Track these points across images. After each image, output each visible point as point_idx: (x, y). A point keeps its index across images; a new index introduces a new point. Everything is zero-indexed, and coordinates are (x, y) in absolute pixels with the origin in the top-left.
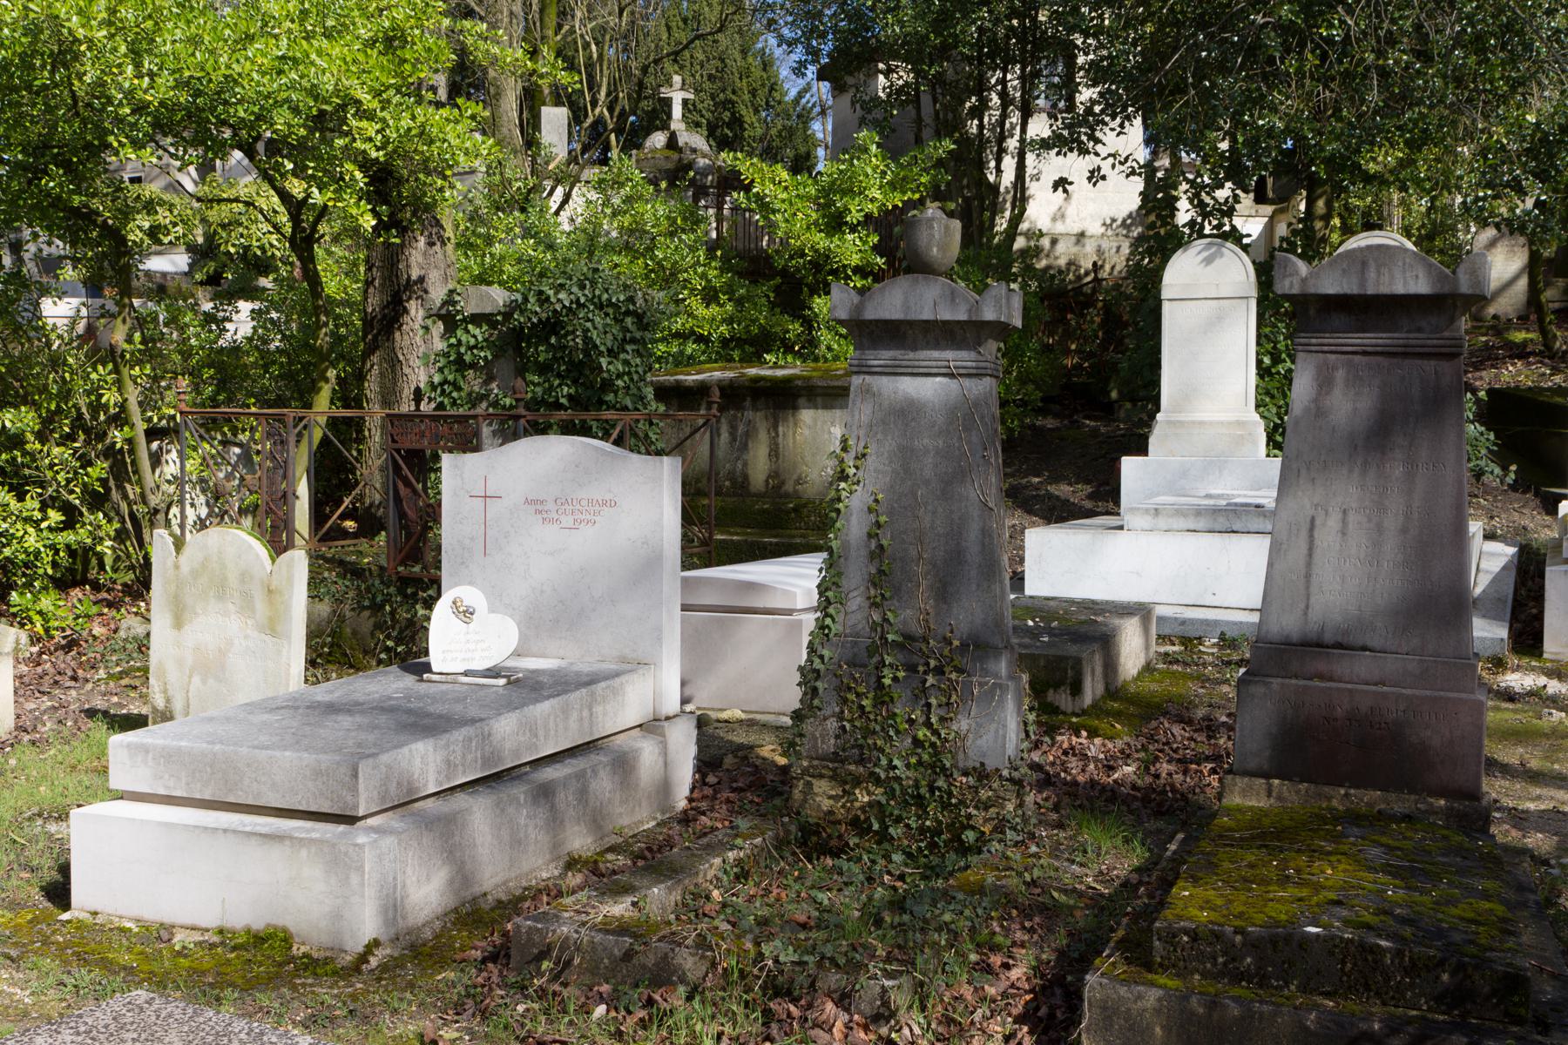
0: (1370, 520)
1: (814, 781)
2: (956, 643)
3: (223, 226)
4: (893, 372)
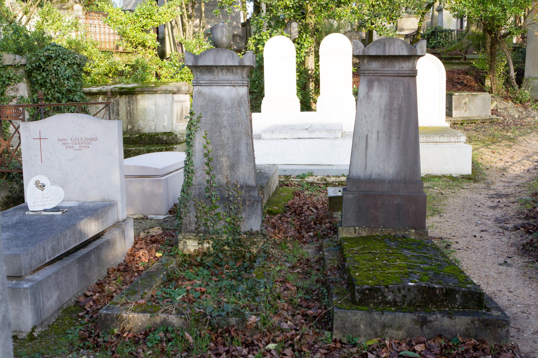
1: (187, 241)
2: (239, 186)
3: (132, 44)
4: (210, 84)
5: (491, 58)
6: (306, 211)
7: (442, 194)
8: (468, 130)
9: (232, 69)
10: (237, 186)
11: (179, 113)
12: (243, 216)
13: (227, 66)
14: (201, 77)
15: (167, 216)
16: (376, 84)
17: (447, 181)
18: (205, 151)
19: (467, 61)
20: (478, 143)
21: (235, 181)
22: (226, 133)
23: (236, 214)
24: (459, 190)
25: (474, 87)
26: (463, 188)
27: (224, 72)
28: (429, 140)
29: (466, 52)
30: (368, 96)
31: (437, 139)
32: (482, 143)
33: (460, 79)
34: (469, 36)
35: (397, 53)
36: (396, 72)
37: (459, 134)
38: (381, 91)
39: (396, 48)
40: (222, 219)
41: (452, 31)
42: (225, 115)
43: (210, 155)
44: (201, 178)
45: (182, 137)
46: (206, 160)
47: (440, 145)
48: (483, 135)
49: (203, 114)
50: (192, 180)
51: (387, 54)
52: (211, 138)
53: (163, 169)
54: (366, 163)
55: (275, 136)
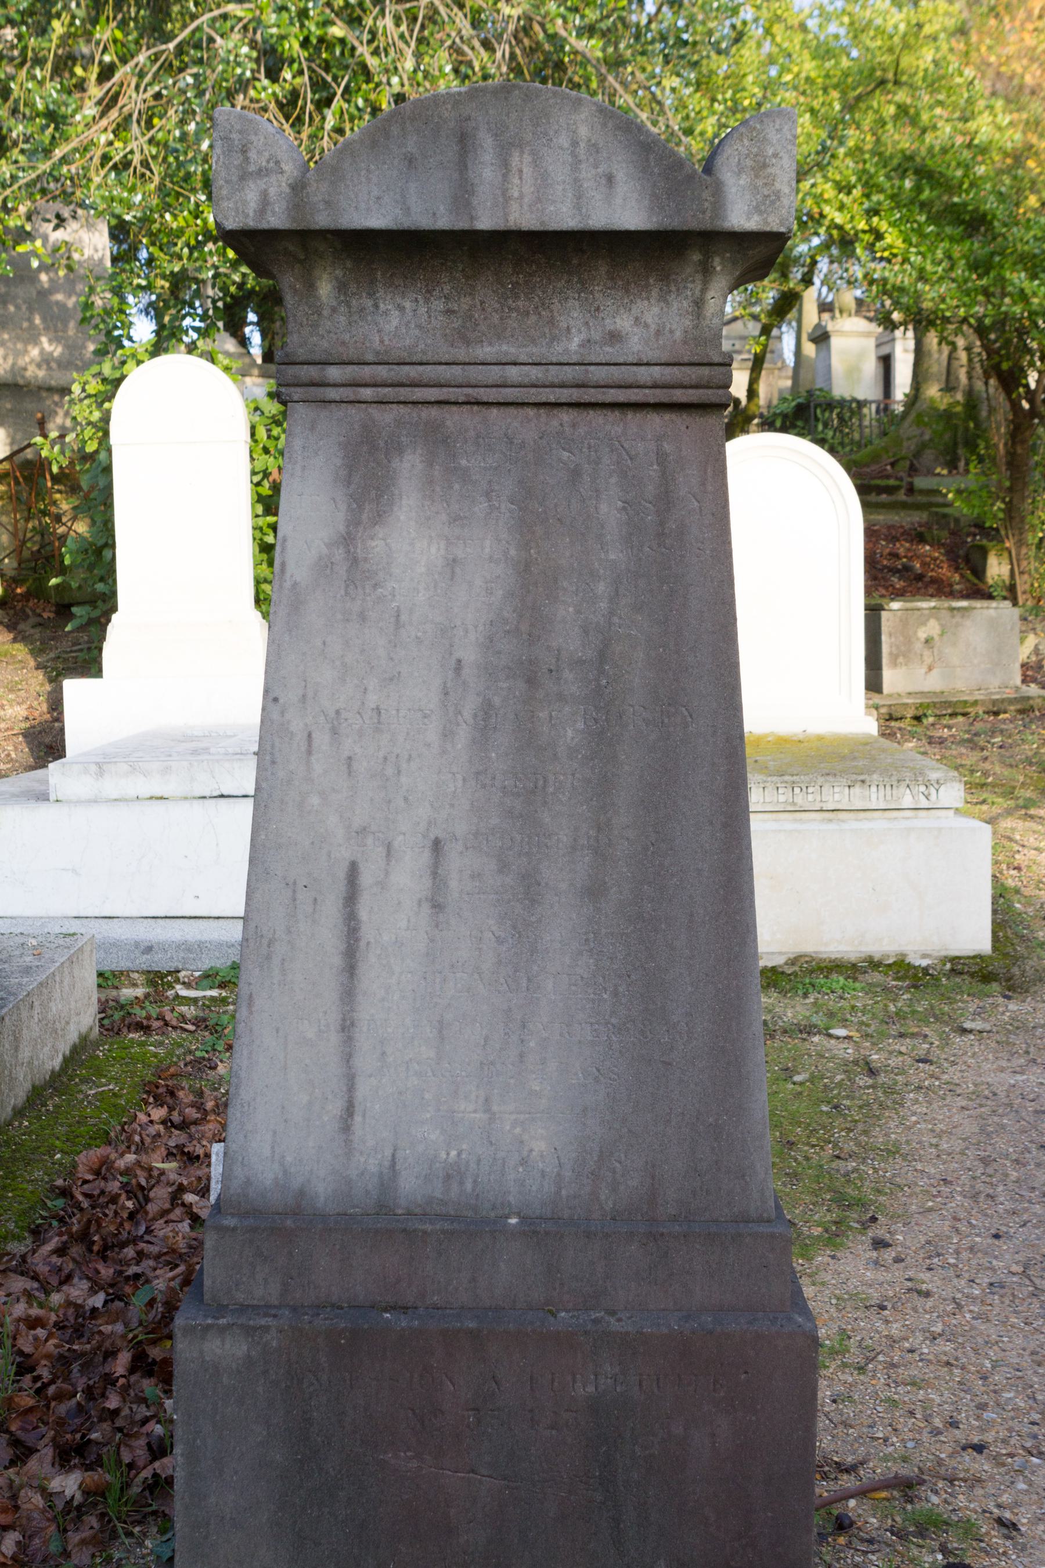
0: (503, 867)
5: (1011, 478)
6: (164, 1213)
7: (872, 1072)
8: (942, 741)
16: (409, 466)
17: (886, 989)
19: (921, 499)
20: (991, 797)
24: (946, 1042)
25: (951, 585)
26: (964, 1031)
28: (800, 799)
29: (913, 470)
30: (352, 564)
31: (837, 795)
32: (1004, 795)
33: (895, 556)
34: (919, 415)
35: (563, 217)
36: (569, 374)
37: (934, 776)
38: (456, 519)
39: (559, 171)
41: (861, 404)
47: (852, 823)
48: (1002, 762)
51: (485, 223)
54: (351, 1088)
55: (110, 787)
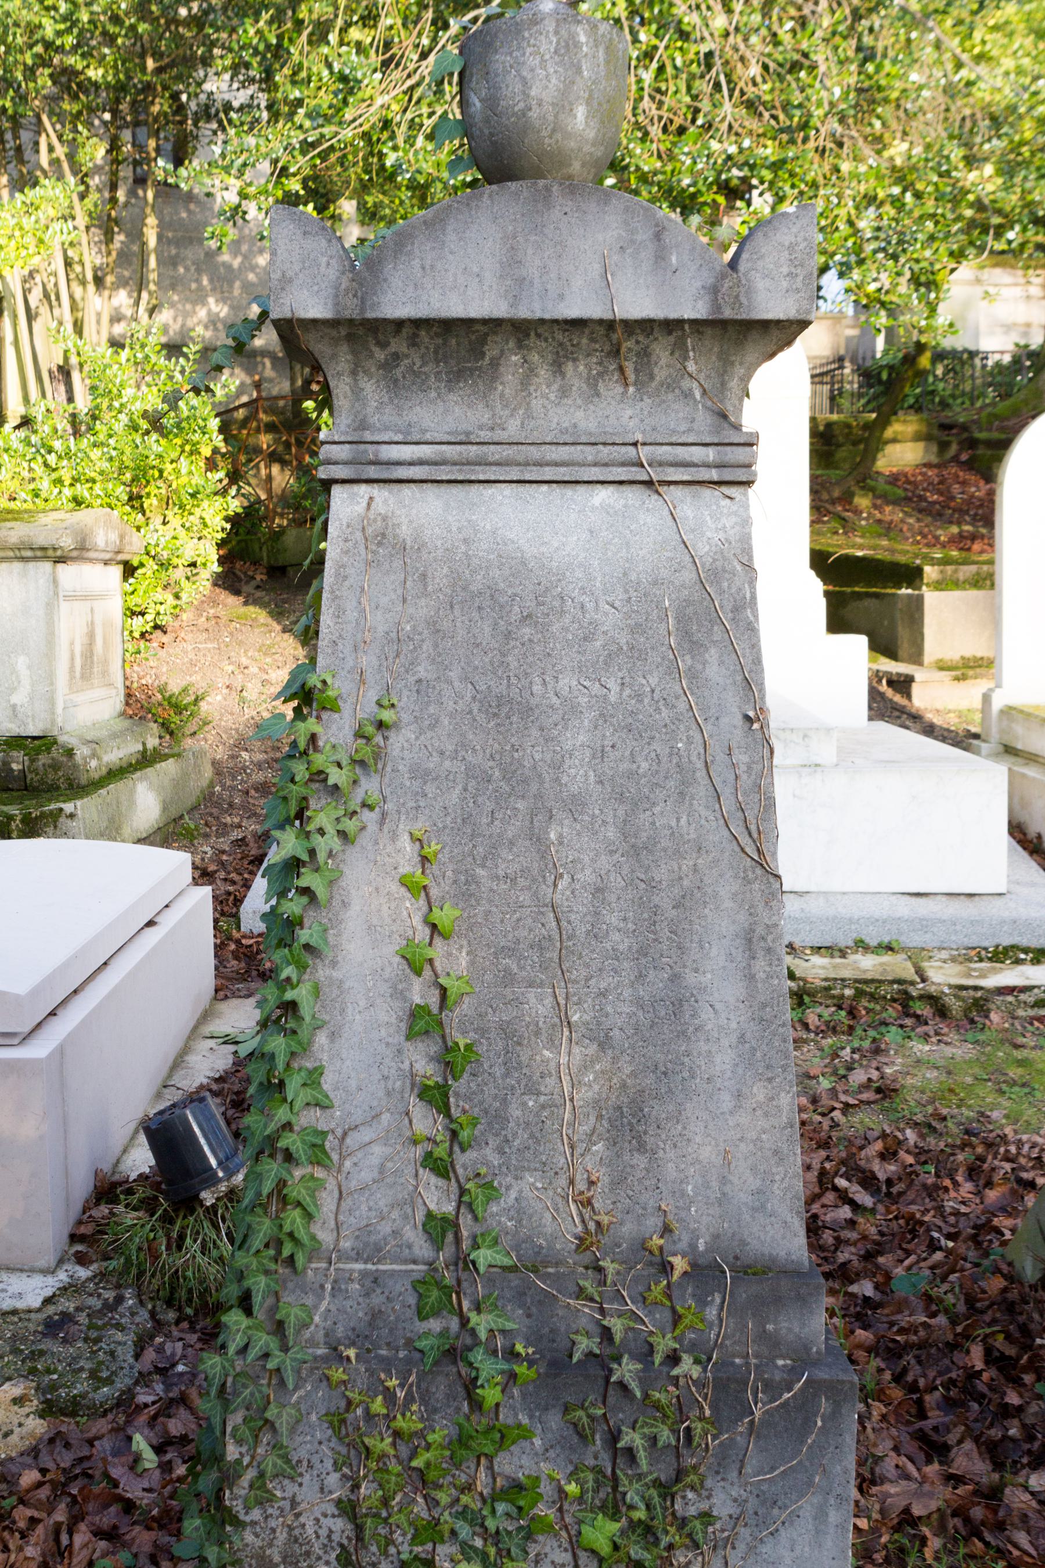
9: (645, 354)
10: (666, 1268)
11: (78, 650)
12: (722, 1505)
13: (609, 325)
14: (389, 415)
15: (62, 1276)
18: (420, 993)
21: (653, 1222)
22: (585, 852)
23: (667, 1490)
27: (576, 372)
40: (549, 1529)
42: (575, 710)
43: (453, 1018)
44: (382, 1199)
45: (94, 755)
46: (426, 1069)
49: (405, 700)
50: (309, 1216)
52: (466, 892)
53: (36, 992)
